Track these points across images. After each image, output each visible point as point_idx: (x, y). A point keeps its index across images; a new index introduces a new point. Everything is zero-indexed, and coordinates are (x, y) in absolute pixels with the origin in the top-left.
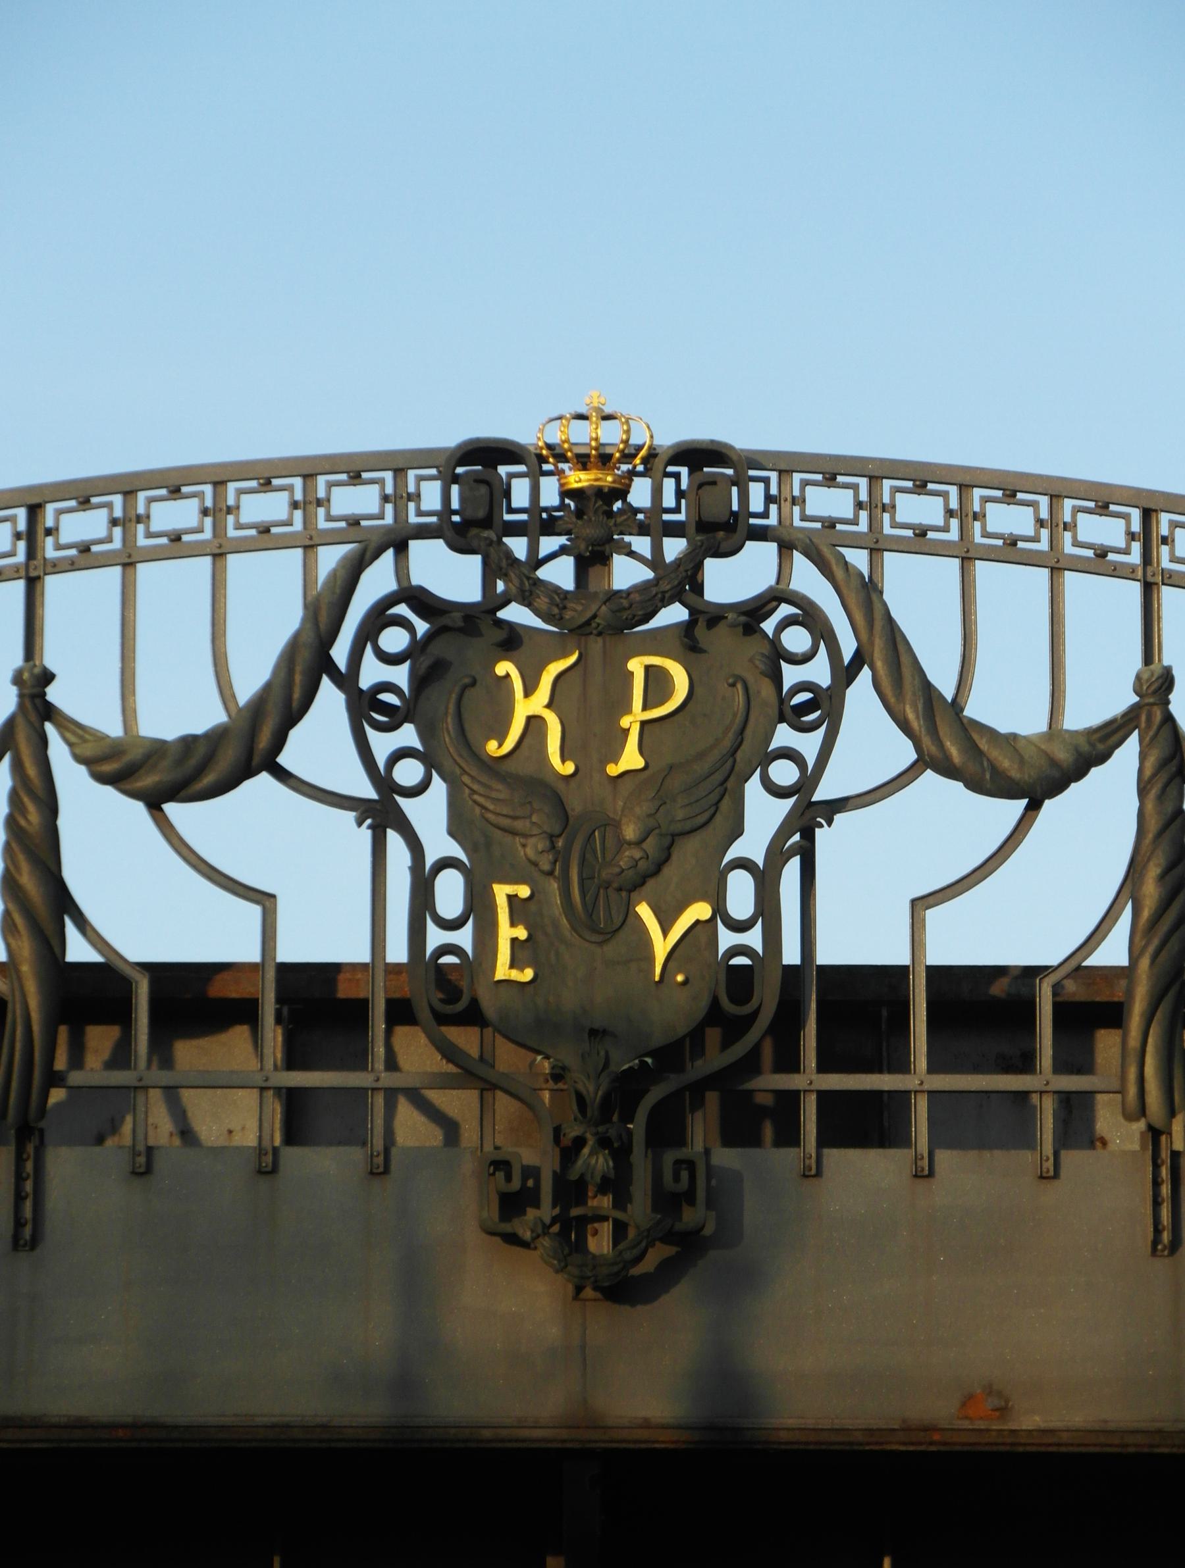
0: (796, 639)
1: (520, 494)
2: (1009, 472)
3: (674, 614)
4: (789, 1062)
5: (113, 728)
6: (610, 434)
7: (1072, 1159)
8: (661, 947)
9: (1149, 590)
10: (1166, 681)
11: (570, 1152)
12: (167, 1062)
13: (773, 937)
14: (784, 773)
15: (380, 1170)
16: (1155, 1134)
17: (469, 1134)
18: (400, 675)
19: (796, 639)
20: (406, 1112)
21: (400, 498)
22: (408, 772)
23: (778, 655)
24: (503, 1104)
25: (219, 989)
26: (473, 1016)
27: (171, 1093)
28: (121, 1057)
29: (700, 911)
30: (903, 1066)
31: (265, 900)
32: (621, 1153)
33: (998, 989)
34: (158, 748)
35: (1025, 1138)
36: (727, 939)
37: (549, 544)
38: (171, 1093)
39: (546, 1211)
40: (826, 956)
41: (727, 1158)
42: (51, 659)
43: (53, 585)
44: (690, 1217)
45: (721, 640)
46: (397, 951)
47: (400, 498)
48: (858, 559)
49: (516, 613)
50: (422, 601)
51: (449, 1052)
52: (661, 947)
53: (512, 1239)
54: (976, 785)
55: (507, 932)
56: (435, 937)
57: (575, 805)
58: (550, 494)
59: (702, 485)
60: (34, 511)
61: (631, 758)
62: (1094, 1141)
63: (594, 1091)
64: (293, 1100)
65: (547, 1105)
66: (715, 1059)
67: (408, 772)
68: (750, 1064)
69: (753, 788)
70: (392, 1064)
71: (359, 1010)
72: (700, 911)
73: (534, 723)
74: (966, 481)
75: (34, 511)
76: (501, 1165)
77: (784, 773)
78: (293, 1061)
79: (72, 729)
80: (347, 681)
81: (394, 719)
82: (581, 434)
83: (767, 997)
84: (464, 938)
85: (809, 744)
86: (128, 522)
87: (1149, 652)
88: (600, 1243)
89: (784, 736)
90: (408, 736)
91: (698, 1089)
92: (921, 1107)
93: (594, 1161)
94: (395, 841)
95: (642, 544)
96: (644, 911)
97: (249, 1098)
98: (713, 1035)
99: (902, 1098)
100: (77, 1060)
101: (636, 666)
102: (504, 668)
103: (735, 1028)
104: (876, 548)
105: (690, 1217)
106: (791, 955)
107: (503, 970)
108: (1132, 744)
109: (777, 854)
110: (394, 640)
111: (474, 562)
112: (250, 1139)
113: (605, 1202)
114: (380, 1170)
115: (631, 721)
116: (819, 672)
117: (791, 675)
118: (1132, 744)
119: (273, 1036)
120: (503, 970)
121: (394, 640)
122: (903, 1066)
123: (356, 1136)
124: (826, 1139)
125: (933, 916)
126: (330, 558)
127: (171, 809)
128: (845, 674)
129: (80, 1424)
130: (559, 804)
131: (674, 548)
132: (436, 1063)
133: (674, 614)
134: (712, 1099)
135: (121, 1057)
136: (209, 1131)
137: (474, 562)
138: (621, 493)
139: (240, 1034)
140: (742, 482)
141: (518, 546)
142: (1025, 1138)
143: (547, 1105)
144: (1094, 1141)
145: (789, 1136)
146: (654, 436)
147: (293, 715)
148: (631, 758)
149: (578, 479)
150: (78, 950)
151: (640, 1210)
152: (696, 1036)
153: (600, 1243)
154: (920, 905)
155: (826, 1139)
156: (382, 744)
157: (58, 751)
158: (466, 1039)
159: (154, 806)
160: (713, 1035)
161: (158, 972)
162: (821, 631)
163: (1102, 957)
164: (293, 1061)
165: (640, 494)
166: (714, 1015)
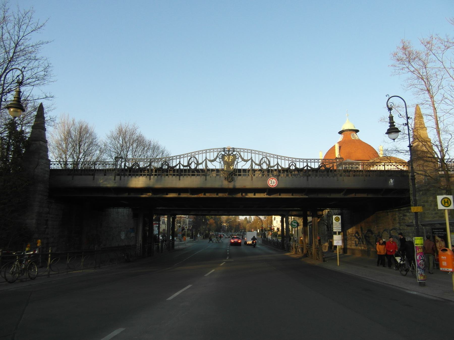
0: (237, 156)
1: (226, 150)
2: (437, 203)
3: (232, 155)
4: (237, 173)
5: (209, 159)
6: (229, 147)
7: (248, 177)
8: (232, 168)
9: (251, 154)
10: (252, 157)
11: (228, 176)
12: (212, 173)
13: (236, 168)
14: (236, 161)
15: (220, 177)
16: (251, 176)
17: (224, 176)
18: (221, 157)
19: (237, 156)
20: (221, 175)
21: (221, 150)
22: (221, 161)
23: (236, 156)
24: (225, 174)
25: (214, 170)
26: (224, 171)
27: (212, 174)
28: (210, 173)
29: (233, 167)
30: (241, 173)
31: (216, 166)
32: (230, 176)
33: (245, 170)
34: (211, 160)
35: (246, 176)
36: (234, 168)
37: (227, 152)
38: (212, 174)
39: (227, 179)
40: (238, 168)
41: (234, 177)
42: (207, 156)
43: (207, 153)
44: (233, 179)
45: (234, 156)
46: (221, 168)
47: (221, 150)
48: (239, 152)
49: (226, 155)
50: (222, 154)
51: (223, 172)
52: (232, 168)
53: (226, 180)
54: (244, 161)
55: (225, 168)
56: (222, 168)
57: (228, 162)
58: (227, 150)
59: (233, 149)
60: (206, 150)
61: (230, 160)
62: (249, 176)
63: (229, 174)
64: (217, 174)
65: (192, 285)
66: (234, 172)
67: (221, 161)
68: (235, 173)
69: (235, 162)
70: (221, 173)
71: (219, 171)
72: (233, 167)
73: (226, 159)
74: (244, 149)
75: (206, 150)
76: (225, 177)
77: (236, 161)
78: (217, 173)
79: (208, 160)
80: (219, 157)
81: (221, 159)
82: (228, 147)
83: (236, 170)
84: (224, 168)
85: (238, 160)
86: (214, 150)
87: (251, 156)
88: (229, 180)
89: (236, 160)
90: (221, 159)
91: (233, 174)
92: (242, 175)
93: (229, 177)
94: (221, 164)
95: (231, 152)
96: (231, 167)
97: (215, 174)
98: (234, 172)
99: (241, 174)
100: (208, 172)
101: (230, 157)
102: (225, 157)
103: (235, 171)
104: (240, 152)
105: (233, 179)
106: (237, 168)
107: (225, 169)
108: (251, 160)
109: (236, 164)
110: (221, 156)
111: (224, 152)
112: (215, 176)
113: (229, 178)
114: (220, 177)
115: (230, 159)
116: (238, 157)
117: (237, 157)
118: (251, 160)
119: (216, 172)
120: (225, 169)
121: (221, 156)
122: (241, 173)
123: (219, 176)
124: (238, 176)
125: (243, 167)
126: (218, 152)
127: (212, 163)
128: (239, 157)
129: (208, 187)
130: (227, 162)
131: (232, 152)
132: (223, 173)
133: (232, 155)
134: (234, 174)
135: (210, 173)
136: (213, 175)
137: (224, 152)
138: (230, 150)
139: (214, 172)
140: (235, 149)
141: (226, 152)
142: (246, 176)
143: (192, 285)
144: (249, 176)
145: (237, 176)
146: (452, 98)
147: (217, 159)
148: (230, 160)
149: (228, 149)
150: (208, 168)
151: (231, 179)
152: (233, 172)
153: (229, 180)
154: (242, 166)
155: (238, 176)
156: (220, 160)
157: (207, 160)
158: (223, 172)
159: (211, 162)
160: (234, 172)
161: (211, 169)
162: (238, 155)
163: (249, 168)
164: (217, 173)
165: (231, 150)
166: (234, 171)
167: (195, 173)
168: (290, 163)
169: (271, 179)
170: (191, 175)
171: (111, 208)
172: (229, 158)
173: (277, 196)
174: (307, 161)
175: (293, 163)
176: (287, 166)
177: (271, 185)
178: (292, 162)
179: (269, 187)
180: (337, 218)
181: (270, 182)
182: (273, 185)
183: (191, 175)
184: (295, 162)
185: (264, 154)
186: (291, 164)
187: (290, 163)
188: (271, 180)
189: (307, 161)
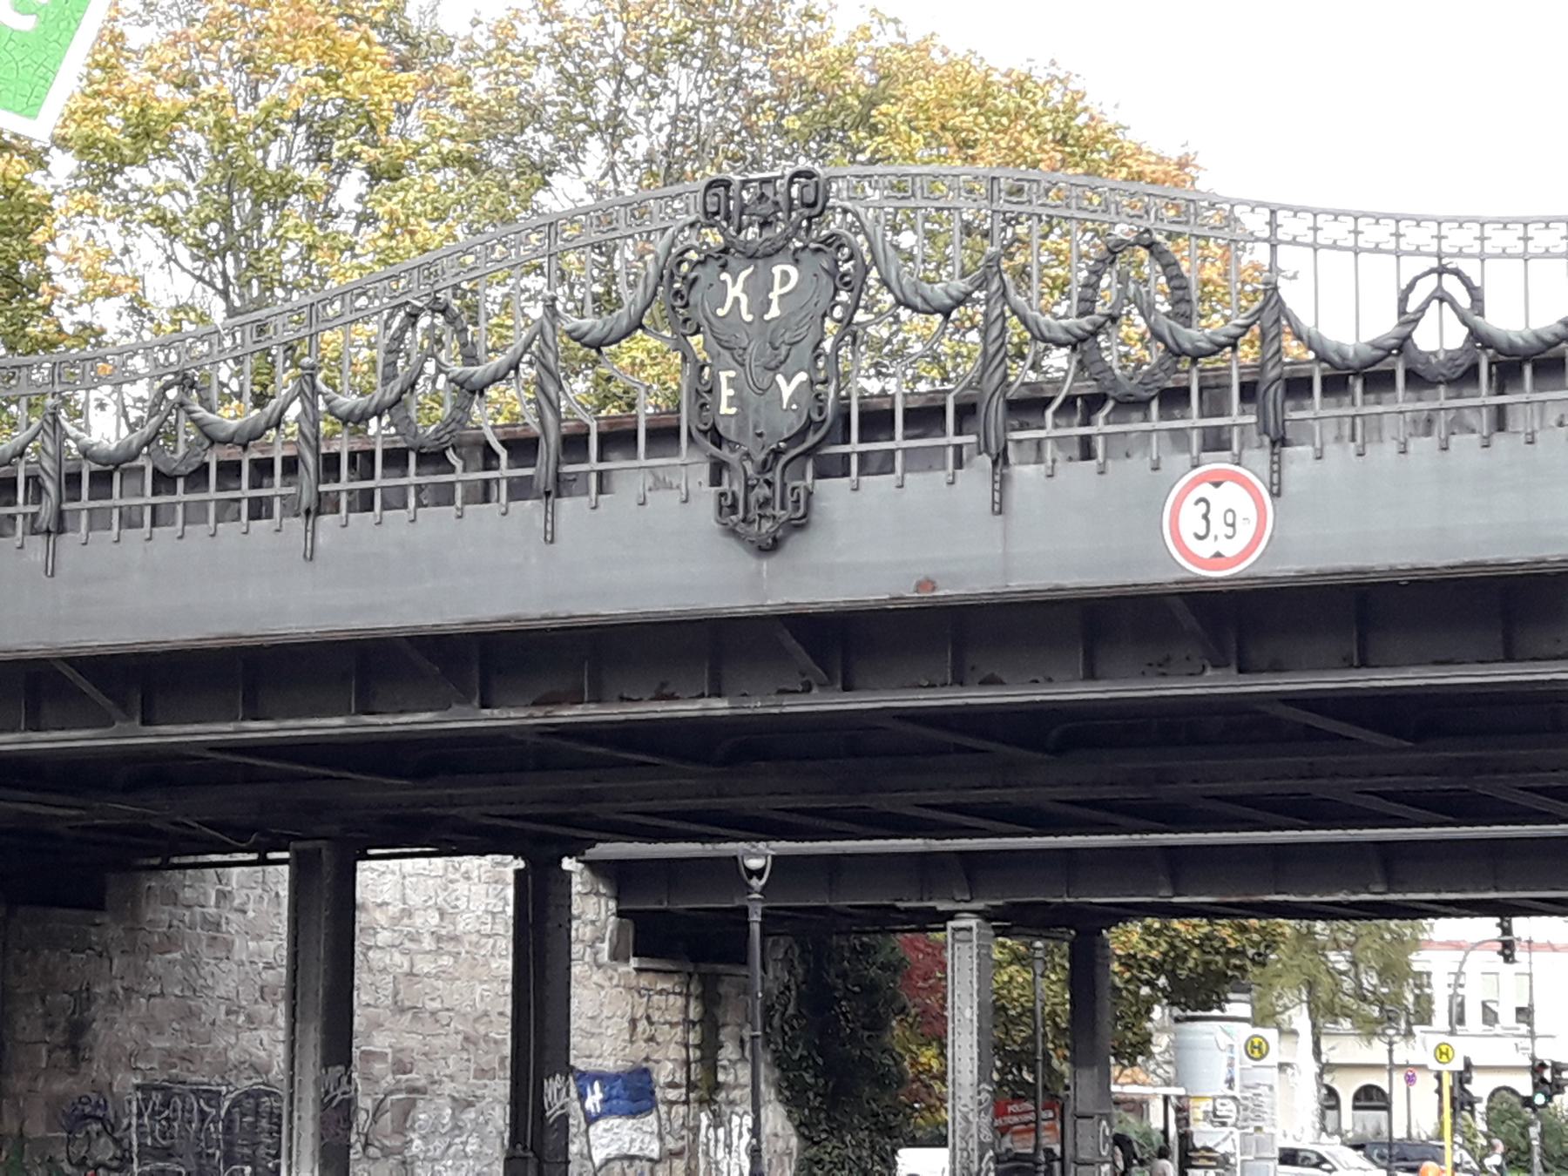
9: (1273, 247)
61: (774, 312)
73: (737, 301)
115: (774, 296)
167: (452, 470)
168: (1411, 287)
169: (1196, 482)
170: (412, 502)
171: (894, 932)
172: (759, 292)
173: (699, 704)
174: (1273, 224)
175: (1452, 285)
176: (1380, 324)
177: (1205, 550)
178: (1441, 271)
179: (1180, 576)
180: (1444, 1058)
181: (1190, 520)
182: (1218, 555)
183: (412, 502)
184: (1470, 268)
185: (1416, 236)
186: (1427, 286)
187: (1411, 287)
188: (1205, 490)
189: (1273, 224)
